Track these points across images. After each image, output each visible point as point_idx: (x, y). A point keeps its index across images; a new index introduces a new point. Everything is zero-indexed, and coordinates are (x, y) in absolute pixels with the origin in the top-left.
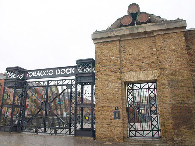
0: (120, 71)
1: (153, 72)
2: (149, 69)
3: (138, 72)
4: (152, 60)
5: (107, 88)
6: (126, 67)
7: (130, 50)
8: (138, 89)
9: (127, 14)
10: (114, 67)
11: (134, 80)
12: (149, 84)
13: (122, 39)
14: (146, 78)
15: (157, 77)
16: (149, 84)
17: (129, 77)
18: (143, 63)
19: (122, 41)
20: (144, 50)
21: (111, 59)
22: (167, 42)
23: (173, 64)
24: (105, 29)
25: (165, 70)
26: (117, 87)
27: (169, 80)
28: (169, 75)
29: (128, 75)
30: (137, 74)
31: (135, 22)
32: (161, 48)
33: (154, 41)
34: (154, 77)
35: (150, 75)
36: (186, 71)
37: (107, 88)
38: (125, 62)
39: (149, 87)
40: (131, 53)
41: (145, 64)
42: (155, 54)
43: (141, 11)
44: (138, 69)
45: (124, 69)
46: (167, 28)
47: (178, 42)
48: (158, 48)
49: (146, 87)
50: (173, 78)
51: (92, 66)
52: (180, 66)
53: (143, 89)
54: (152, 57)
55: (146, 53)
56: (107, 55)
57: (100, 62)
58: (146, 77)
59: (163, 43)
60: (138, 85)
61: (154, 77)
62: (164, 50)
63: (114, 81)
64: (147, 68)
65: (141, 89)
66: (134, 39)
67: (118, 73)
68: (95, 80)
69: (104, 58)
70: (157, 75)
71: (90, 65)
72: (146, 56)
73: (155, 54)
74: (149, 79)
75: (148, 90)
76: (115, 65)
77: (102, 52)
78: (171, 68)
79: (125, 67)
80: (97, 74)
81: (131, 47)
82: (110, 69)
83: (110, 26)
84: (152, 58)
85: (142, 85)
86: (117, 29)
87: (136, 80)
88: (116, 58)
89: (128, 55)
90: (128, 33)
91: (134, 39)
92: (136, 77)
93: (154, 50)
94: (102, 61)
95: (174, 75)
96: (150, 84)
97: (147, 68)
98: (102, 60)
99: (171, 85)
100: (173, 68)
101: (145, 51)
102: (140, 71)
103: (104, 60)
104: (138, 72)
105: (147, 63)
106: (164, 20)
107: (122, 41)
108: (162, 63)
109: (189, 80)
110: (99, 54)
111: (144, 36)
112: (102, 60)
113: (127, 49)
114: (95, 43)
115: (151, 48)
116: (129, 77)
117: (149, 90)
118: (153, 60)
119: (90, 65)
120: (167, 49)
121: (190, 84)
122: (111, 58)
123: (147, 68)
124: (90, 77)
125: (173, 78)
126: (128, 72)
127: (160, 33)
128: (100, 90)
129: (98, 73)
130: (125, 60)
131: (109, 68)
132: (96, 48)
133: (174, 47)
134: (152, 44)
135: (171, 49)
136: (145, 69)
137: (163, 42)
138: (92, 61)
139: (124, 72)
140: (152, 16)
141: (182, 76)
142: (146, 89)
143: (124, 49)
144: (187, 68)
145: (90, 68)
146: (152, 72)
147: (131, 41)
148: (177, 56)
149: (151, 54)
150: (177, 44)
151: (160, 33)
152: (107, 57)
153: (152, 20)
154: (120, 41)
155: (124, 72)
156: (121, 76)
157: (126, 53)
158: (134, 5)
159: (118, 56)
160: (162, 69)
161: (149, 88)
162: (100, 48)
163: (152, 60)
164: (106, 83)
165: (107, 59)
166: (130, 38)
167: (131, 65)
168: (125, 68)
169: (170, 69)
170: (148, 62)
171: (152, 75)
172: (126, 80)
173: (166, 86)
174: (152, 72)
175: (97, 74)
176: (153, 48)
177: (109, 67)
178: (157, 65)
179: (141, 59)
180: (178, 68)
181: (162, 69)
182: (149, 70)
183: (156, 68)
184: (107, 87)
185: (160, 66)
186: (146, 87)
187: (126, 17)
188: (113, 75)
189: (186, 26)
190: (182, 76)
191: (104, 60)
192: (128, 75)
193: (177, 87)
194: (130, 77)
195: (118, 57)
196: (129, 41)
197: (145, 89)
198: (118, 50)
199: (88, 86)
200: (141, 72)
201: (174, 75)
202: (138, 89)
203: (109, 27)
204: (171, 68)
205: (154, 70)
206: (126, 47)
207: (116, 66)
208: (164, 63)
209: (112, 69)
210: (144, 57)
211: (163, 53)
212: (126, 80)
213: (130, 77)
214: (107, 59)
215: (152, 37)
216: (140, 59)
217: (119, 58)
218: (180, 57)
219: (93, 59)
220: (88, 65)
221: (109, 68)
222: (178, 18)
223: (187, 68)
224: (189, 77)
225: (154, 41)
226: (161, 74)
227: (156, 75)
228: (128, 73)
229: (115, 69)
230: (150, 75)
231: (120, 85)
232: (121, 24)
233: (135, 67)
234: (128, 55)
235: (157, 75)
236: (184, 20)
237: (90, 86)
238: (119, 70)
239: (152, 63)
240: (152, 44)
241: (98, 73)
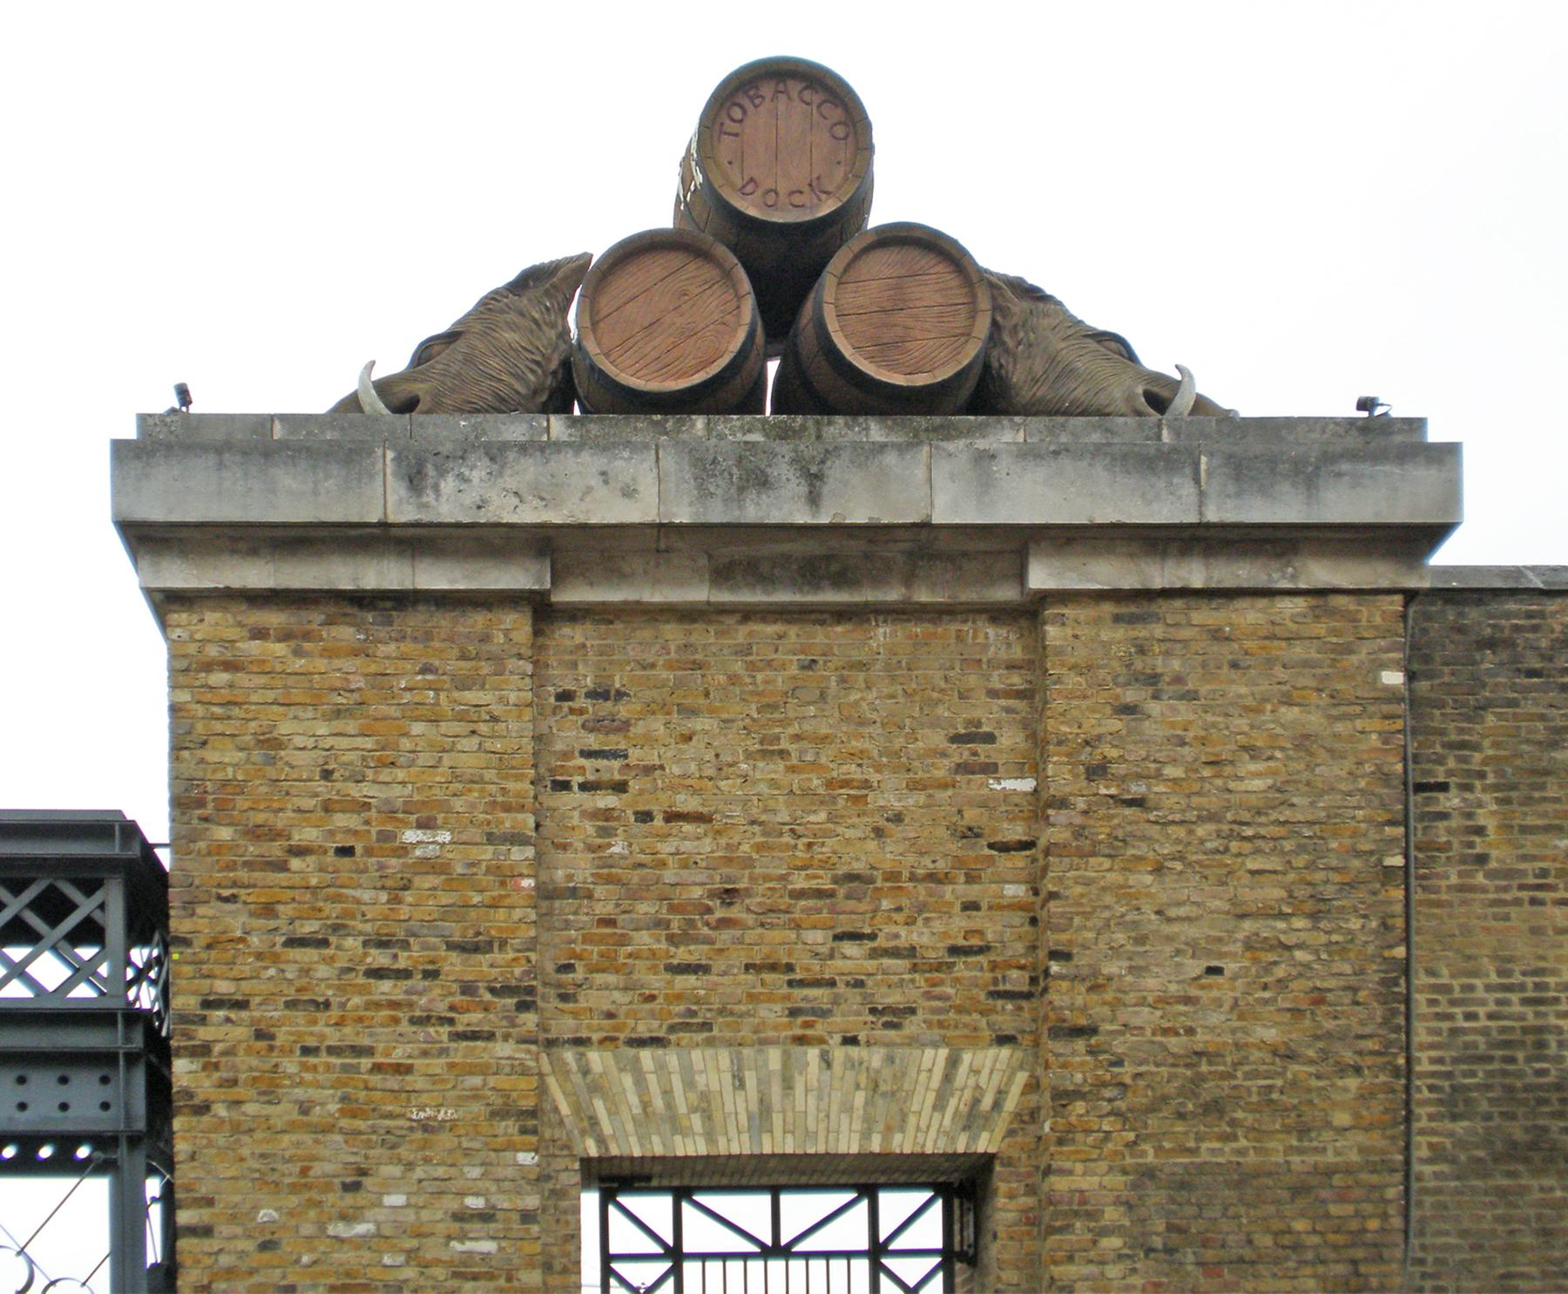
0: (529, 1020)
1: (963, 1069)
2: (912, 1026)
3: (774, 1056)
4: (959, 922)
5: (338, 1229)
6: (611, 978)
7: (681, 763)
8: (745, 1256)
9: (664, 219)
10: (454, 964)
11: (710, 1137)
12: (885, 1198)
13: (575, 594)
14: (866, 1135)
15: (1002, 1123)
16: (885, 1198)
17: (646, 1105)
18: (850, 948)
19: (576, 614)
20: (866, 784)
21: (404, 850)
22: (1185, 712)
23: (1222, 989)
24: (319, 400)
25: (1119, 1046)
26: (486, 1216)
27: (1149, 1173)
28: (1151, 1109)
29: (640, 1081)
30: (750, 1078)
31: (773, 367)
32: (1097, 771)
33: (1017, 680)
34: (972, 1119)
35: (923, 1100)
36: (1352, 1083)
37: (338, 1229)
38: (603, 909)
39: (657, 1249)
40: (687, 802)
41: (871, 965)
42: (1004, 848)
43: (879, 215)
44: (772, 1013)
45: (587, 999)
46: (1212, 516)
47: (1314, 721)
48: (1062, 776)
49: (852, 1231)
50: (1193, 1152)
51: (115, 922)
52: (1296, 1012)
53: (807, 1255)
54: (971, 879)
55: (898, 818)
56: (356, 791)
57: (243, 875)
58: (869, 1120)
59: (1128, 710)
60: (751, 1210)
61: (972, 1119)
62: (1138, 802)
63: (446, 1140)
64: (893, 1016)
65: (776, 1250)
66: (748, 614)
67: (503, 1049)
68: (168, 1118)
69: (307, 835)
70: (1010, 1105)
71: (86, 907)
72: (890, 854)
73: (1004, 848)
74: (903, 1143)
75: (862, 1267)
76: (456, 931)
77: (271, 743)
78: (1190, 1031)
79: (599, 978)
80: (203, 1034)
81: (693, 712)
82: (386, 986)
83: (395, 361)
84: (973, 892)
85: (800, 1209)
86: (515, 429)
87: (736, 1144)
88: (487, 853)
89: (645, 817)
90: (683, 516)
91: (748, 614)
92: (738, 1106)
93: (1007, 795)
94: (282, 867)
95: (1215, 1108)
96: (895, 1205)
97: (893, 1016)
98: (275, 850)
99: (1160, 1225)
100: (1213, 1027)
101: (890, 795)
102: (801, 1040)
103: (300, 851)
104: (774, 1056)
105: (894, 953)
106: (1182, 403)
107: (576, 614)
108: (1082, 960)
109: (1365, 1177)
110: (226, 758)
111: (892, 594)
112: (275, 850)
113: (649, 740)
114: (166, 603)
115: (963, 768)
116: (646, 1105)
117: (877, 1269)
118: (978, 920)
119: (86, 907)
120: (1171, 803)
121: (1373, 1224)
122: (411, 836)
123: (887, 1010)
124: (93, 1076)
125: (1193, 1152)
126: (640, 1043)
127: (1106, 573)
128: (248, 1245)
129: (218, 1030)
130: (610, 880)
131: (378, 973)
132: (183, 670)
133: (1254, 780)
134: (989, 713)
135: (1213, 802)
136: (850, 1016)
137: (1130, 696)
138: (113, 849)
139: (579, 1042)
140: (1019, 307)
141: (1303, 1131)
142: (848, 1255)
143: (593, 741)
144: (1370, 1045)
145: (86, 953)
146: (953, 1063)
147: (703, 636)
148: (1273, 893)
149: (954, 847)
150: (1304, 742)
151: (1106, 573)
152: (341, 820)
153: (1017, 375)
154: (543, 610)
155: (579, 1042)
156: (542, 1090)
157: (620, 787)
158: (836, 114)
159: (508, 822)
160: (1078, 1032)
161: (877, 1251)
162: (241, 678)
163: (959, 922)
164: (334, 1157)
165: (346, 851)
166: (699, 593)
167: (682, 955)
168: (604, 993)
169: (1175, 1043)
170: (917, 936)
171: (939, 1105)
172: (601, 1141)
173: (1106, 1232)
174: (953, 1063)
175: (203, 1034)
176: (990, 769)
177: (379, 958)
178: (1017, 979)
179: (819, 894)
180: (1271, 1035)
181: (1078, 1032)
182: (913, 1042)
183: (1007, 1024)
184: (344, 1217)
185: (1065, 998)
186: (852, 1231)
187: (657, 266)
188: (437, 1065)
189: (1436, 533)
190: (1303, 1131)
191: (300, 851)
192: (640, 1081)
193: (1235, 1252)
194: (658, 1103)
195: (517, 839)
196: (672, 632)
197: (827, 1255)
198: (517, 733)
199: (74, 1181)
200: (813, 1053)
201: (1215, 1108)
202: (745, 1256)
203: (377, 374)
204: (1190, 1031)
205: (973, 1040)
206: (623, 710)
207: (476, 949)
208: (1112, 968)
209: (417, 982)
210: (859, 867)
211: (1116, 846)
212: (601, 1141)
213: (658, 1103)
214: (346, 851)
215: (998, 614)
216: (799, 894)
217: (520, 854)
218: (1314, 916)
219: (131, 830)
220: (53, 907)
221: (378, 973)
222: (1366, 404)
223: (1370, 1045)
224: (1376, 1140)
225: (1017, 680)
226: (1063, 1097)
227: (997, 1105)
228: (646, 1056)
229: (468, 989)
230: (923, 1100)
231: (532, 1201)
232: (566, 365)
233: (731, 983)
234: (645, 817)
235: (1010, 1105)
236: (1434, 435)
237: (97, 1190)
238: (523, 1007)
239: (954, 950)
240: (989, 713)
241: (218, 1030)
